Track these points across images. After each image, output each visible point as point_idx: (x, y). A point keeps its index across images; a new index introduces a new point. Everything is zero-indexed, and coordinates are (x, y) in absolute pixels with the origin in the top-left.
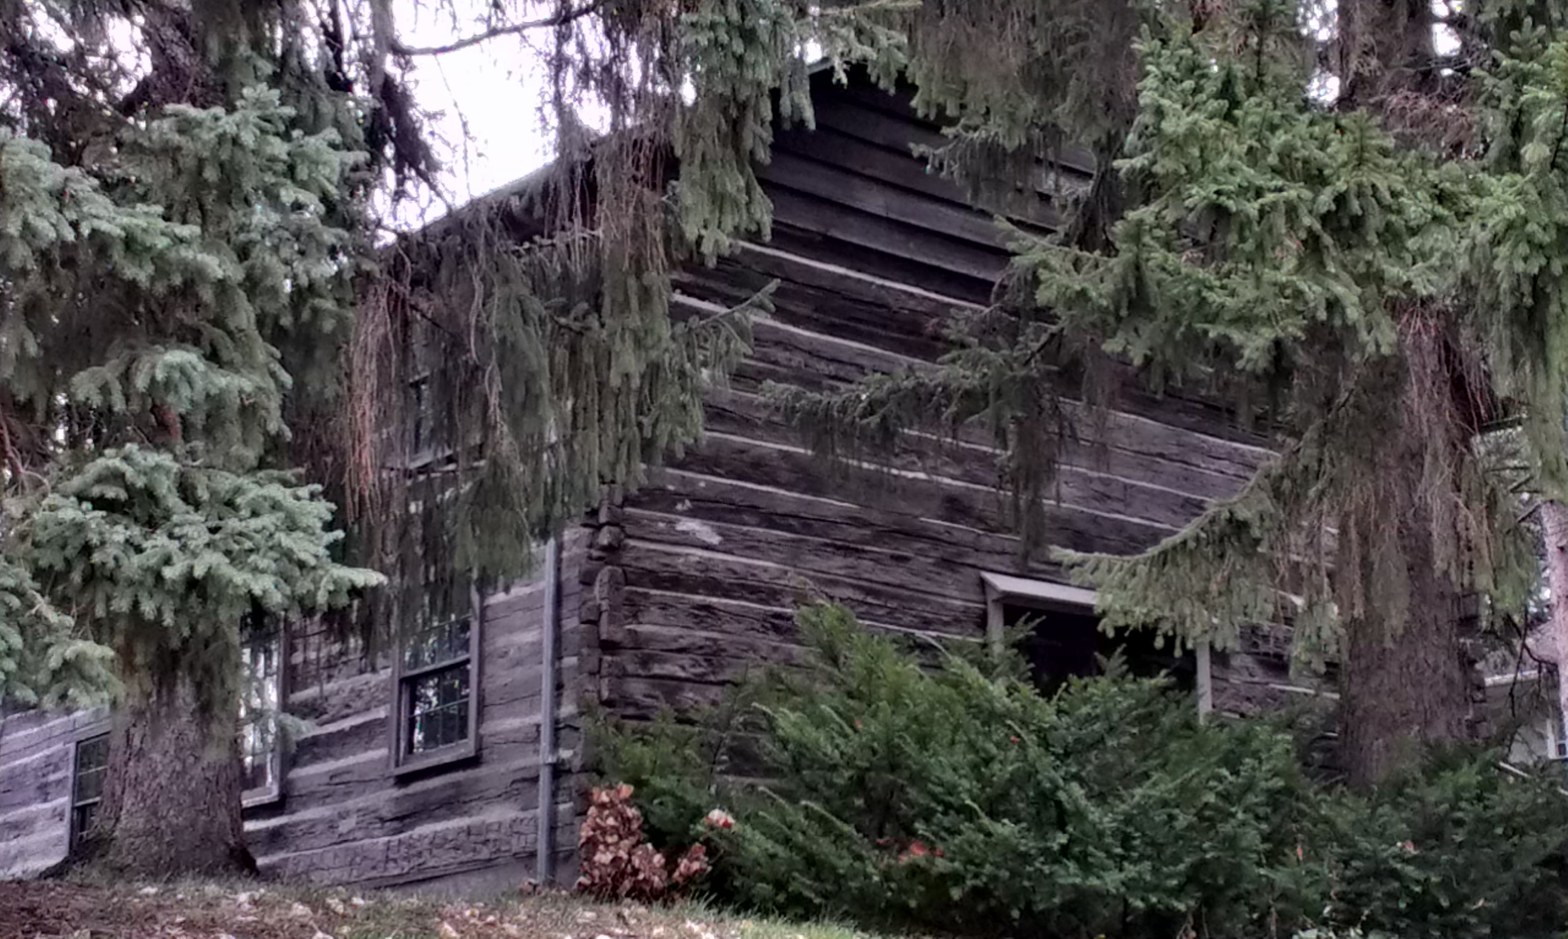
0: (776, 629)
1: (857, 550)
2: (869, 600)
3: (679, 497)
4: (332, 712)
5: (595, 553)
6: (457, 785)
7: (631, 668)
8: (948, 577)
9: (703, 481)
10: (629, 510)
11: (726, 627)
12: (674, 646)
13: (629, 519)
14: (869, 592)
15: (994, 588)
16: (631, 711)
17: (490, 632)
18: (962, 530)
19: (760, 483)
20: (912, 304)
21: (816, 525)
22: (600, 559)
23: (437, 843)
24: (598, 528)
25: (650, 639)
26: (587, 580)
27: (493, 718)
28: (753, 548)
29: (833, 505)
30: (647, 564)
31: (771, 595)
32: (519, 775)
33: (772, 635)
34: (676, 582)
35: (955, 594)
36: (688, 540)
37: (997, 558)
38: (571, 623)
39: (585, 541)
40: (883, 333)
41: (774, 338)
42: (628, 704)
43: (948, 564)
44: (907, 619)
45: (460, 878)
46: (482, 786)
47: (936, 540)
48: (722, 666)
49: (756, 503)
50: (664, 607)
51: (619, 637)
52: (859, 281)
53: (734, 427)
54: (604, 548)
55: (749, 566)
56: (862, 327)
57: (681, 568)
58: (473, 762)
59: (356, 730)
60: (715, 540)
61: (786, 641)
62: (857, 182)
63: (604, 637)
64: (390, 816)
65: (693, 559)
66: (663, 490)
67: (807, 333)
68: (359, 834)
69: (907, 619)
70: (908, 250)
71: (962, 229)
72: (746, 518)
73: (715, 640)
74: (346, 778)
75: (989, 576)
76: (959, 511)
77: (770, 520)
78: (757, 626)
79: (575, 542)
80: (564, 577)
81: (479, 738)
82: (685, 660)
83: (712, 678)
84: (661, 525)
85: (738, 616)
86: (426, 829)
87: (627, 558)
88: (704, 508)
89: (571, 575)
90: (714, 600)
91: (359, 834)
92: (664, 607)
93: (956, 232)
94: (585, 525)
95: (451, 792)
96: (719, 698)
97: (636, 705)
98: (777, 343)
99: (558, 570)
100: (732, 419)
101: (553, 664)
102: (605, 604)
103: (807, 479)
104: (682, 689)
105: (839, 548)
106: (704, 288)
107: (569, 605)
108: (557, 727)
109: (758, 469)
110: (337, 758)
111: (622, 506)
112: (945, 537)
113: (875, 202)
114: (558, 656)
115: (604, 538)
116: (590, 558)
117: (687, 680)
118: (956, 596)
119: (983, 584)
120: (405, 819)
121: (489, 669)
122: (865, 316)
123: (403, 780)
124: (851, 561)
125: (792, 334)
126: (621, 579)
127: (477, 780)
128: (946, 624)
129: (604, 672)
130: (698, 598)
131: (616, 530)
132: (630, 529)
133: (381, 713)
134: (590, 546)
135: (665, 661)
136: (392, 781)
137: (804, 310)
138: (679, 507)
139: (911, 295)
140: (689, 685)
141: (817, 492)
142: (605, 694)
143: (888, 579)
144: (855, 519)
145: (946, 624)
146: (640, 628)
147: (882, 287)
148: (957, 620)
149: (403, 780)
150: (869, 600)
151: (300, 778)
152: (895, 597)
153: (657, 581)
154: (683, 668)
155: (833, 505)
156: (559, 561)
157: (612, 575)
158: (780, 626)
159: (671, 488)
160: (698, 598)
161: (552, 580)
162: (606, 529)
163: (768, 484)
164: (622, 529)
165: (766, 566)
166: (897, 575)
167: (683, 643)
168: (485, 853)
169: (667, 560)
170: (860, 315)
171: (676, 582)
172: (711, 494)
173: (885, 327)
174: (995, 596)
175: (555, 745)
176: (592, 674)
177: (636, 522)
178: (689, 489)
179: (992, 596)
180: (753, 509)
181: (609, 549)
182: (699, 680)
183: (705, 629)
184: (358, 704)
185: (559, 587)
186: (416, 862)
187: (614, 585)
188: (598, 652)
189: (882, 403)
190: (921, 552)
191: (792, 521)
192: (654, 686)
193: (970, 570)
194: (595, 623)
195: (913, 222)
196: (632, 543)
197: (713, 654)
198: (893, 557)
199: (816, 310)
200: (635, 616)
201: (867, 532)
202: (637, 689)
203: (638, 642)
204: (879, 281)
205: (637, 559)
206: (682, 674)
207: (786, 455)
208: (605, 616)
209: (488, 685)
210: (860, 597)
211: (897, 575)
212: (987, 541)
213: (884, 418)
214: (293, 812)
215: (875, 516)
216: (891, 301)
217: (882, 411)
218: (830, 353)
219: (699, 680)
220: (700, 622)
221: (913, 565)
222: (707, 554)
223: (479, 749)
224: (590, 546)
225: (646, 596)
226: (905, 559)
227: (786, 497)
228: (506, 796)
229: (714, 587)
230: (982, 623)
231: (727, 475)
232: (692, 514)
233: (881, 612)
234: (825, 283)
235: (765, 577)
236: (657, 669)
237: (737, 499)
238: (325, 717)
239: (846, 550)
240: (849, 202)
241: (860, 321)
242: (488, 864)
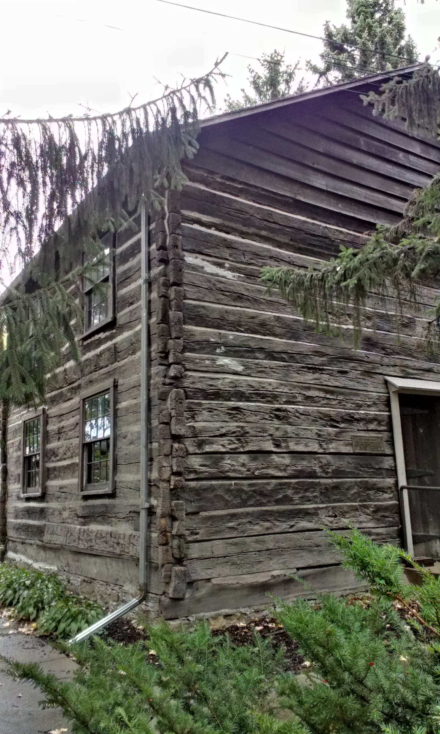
0: (278, 417)
1: (320, 370)
2: (328, 396)
3: (218, 345)
4: (60, 456)
5: (168, 381)
6: (106, 506)
7: (191, 449)
8: (368, 381)
9: (231, 335)
10: (188, 354)
11: (248, 419)
12: (218, 433)
13: (186, 359)
14: (327, 392)
15: (394, 385)
16: (192, 476)
17: (120, 423)
18: (374, 355)
19: (265, 335)
20: (341, 237)
21: (298, 357)
22: (170, 384)
23: (100, 536)
24: (169, 365)
25: (204, 430)
26: (163, 397)
27: (121, 472)
28: (262, 372)
29: (306, 345)
30: (199, 386)
31: (274, 398)
32: (132, 509)
33: (276, 421)
34: (217, 395)
35: (372, 389)
36: (224, 371)
37: (392, 368)
38: (155, 423)
39: (162, 374)
40: (326, 252)
41: (268, 254)
42: (191, 472)
43: (368, 373)
44: (349, 405)
45: (108, 560)
46: (116, 510)
47: (360, 361)
48: (247, 442)
49: (263, 346)
50: (210, 410)
51: (183, 431)
52: (313, 224)
53: (248, 304)
54: (172, 378)
55: (259, 382)
56: (316, 249)
57: (221, 387)
58: (112, 495)
59: (68, 467)
60: (240, 369)
61: (284, 424)
62: (310, 171)
63: (173, 432)
64: (80, 515)
65: (227, 381)
66: (208, 341)
67: (287, 252)
68: (70, 521)
69: (349, 405)
70: (339, 208)
71: (365, 197)
72: (257, 355)
73: (242, 427)
74: (65, 490)
75: (389, 379)
76: (371, 345)
77: (271, 355)
78: (267, 417)
79: (157, 374)
80: (151, 395)
81: (114, 482)
82: (225, 441)
83: (241, 450)
84: (207, 362)
85: (255, 412)
86: (94, 527)
87: (186, 383)
88: (233, 351)
89: (154, 394)
90: (240, 404)
91: (70, 521)
92: (210, 410)
93: (362, 200)
94: (161, 364)
95: (104, 509)
96: (246, 462)
97: (195, 472)
98: (271, 258)
99: (149, 390)
100: (248, 300)
101: (146, 447)
102: (173, 413)
103: (292, 332)
104: (223, 459)
105: (309, 368)
106: (227, 227)
107: (155, 411)
108: (150, 484)
109: (263, 327)
110: (63, 479)
111: (183, 351)
112: (366, 359)
113: (320, 182)
114: (150, 440)
115: (172, 372)
116: (164, 384)
117: (227, 453)
118: (373, 389)
119: (386, 382)
120: (87, 518)
121: (119, 444)
122: (318, 243)
123: (86, 498)
124: (317, 375)
125: (279, 253)
126: (183, 396)
127: (114, 506)
128: (369, 406)
129: (174, 454)
130: (231, 404)
131: (180, 367)
132: (188, 366)
133: (77, 460)
134: (165, 377)
135: (212, 443)
136: (80, 497)
137: (285, 240)
138: (218, 351)
139: (341, 232)
140: (228, 456)
141: (297, 339)
142: (175, 469)
143: (337, 384)
144: (316, 352)
145: (369, 406)
146: (196, 425)
147: (326, 227)
148: (375, 404)
149: (86, 498)
150: (328, 396)
151: (52, 486)
152: (342, 394)
153: (207, 395)
154: (223, 446)
155: (306, 345)
156: (149, 385)
157: (177, 393)
158: (280, 416)
159: (212, 340)
160: (231, 404)
161: (145, 397)
162: (172, 366)
163: (269, 335)
164: (183, 366)
165: (270, 382)
166: (342, 381)
167: (223, 431)
168: (118, 551)
169: (211, 383)
170: (314, 243)
171: (217, 395)
172: (237, 343)
173: (327, 249)
174: (394, 389)
175: (149, 494)
176: (166, 455)
177: (192, 361)
178: (223, 340)
179: (392, 390)
180: (261, 350)
181: (175, 378)
182: (234, 452)
183: (236, 421)
184: (69, 454)
185: (149, 400)
186: (90, 544)
187: (179, 400)
188: (170, 441)
189: (356, 269)
190: (354, 368)
191: (284, 356)
192: (205, 459)
193: (381, 376)
194: (168, 424)
195: (340, 193)
196: (189, 373)
197: (242, 436)
198: (339, 372)
199: (291, 240)
200: (193, 417)
201: (324, 359)
202: (195, 462)
203: (195, 433)
204: (324, 225)
205: (193, 383)
206: (223, 450)
207: (278, 319)
208: (173, 419)
209: (120, 454)
210: (322, 395)
211: (342, 381)
212: (386, 360)
213: (359, 280)
214: (48, 502)
215: (329, 351)
216: (330, 235)
217: (358, 274)
218: (300, 263)
219: (234, 452)
220: (232, 417)
221: (351, 375)
222: (236, 377)
223: (115, 489)
224: (165, 377)
225: (200, 404)
226: (345, 372)
227: (279, 343)
228: (127, 519)
229: (241, 396)
230: (388, 404)
231: (246, 331)
232: (226, 354)
233: (334, 402)
234: (296, 225)
235: (270, 388)
236: (208, 448)
237: (252, 344)
238: (58, 458)
239: (314, 369)
240: (307, 182)
241: (314, 246)
242: (119, 557)
